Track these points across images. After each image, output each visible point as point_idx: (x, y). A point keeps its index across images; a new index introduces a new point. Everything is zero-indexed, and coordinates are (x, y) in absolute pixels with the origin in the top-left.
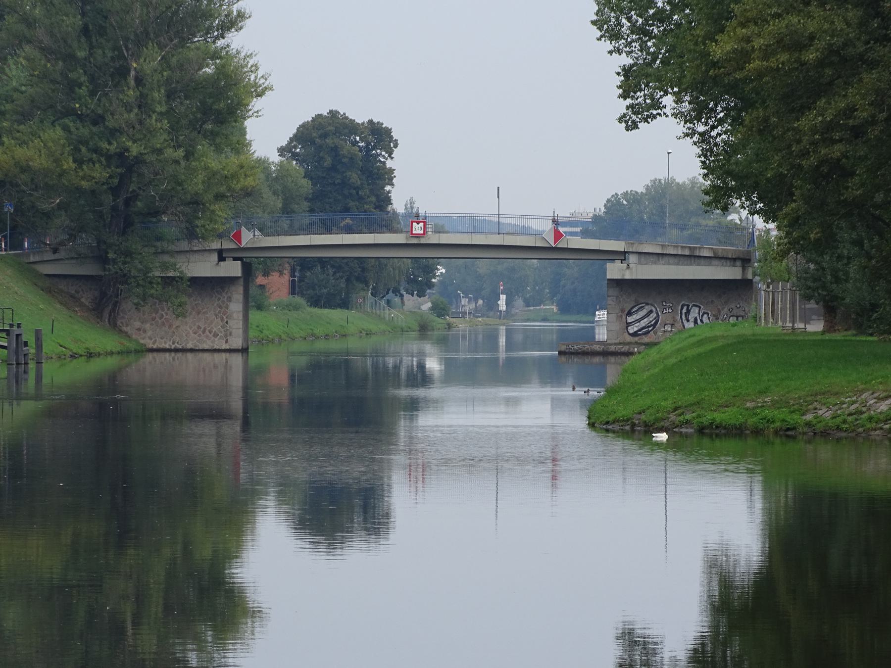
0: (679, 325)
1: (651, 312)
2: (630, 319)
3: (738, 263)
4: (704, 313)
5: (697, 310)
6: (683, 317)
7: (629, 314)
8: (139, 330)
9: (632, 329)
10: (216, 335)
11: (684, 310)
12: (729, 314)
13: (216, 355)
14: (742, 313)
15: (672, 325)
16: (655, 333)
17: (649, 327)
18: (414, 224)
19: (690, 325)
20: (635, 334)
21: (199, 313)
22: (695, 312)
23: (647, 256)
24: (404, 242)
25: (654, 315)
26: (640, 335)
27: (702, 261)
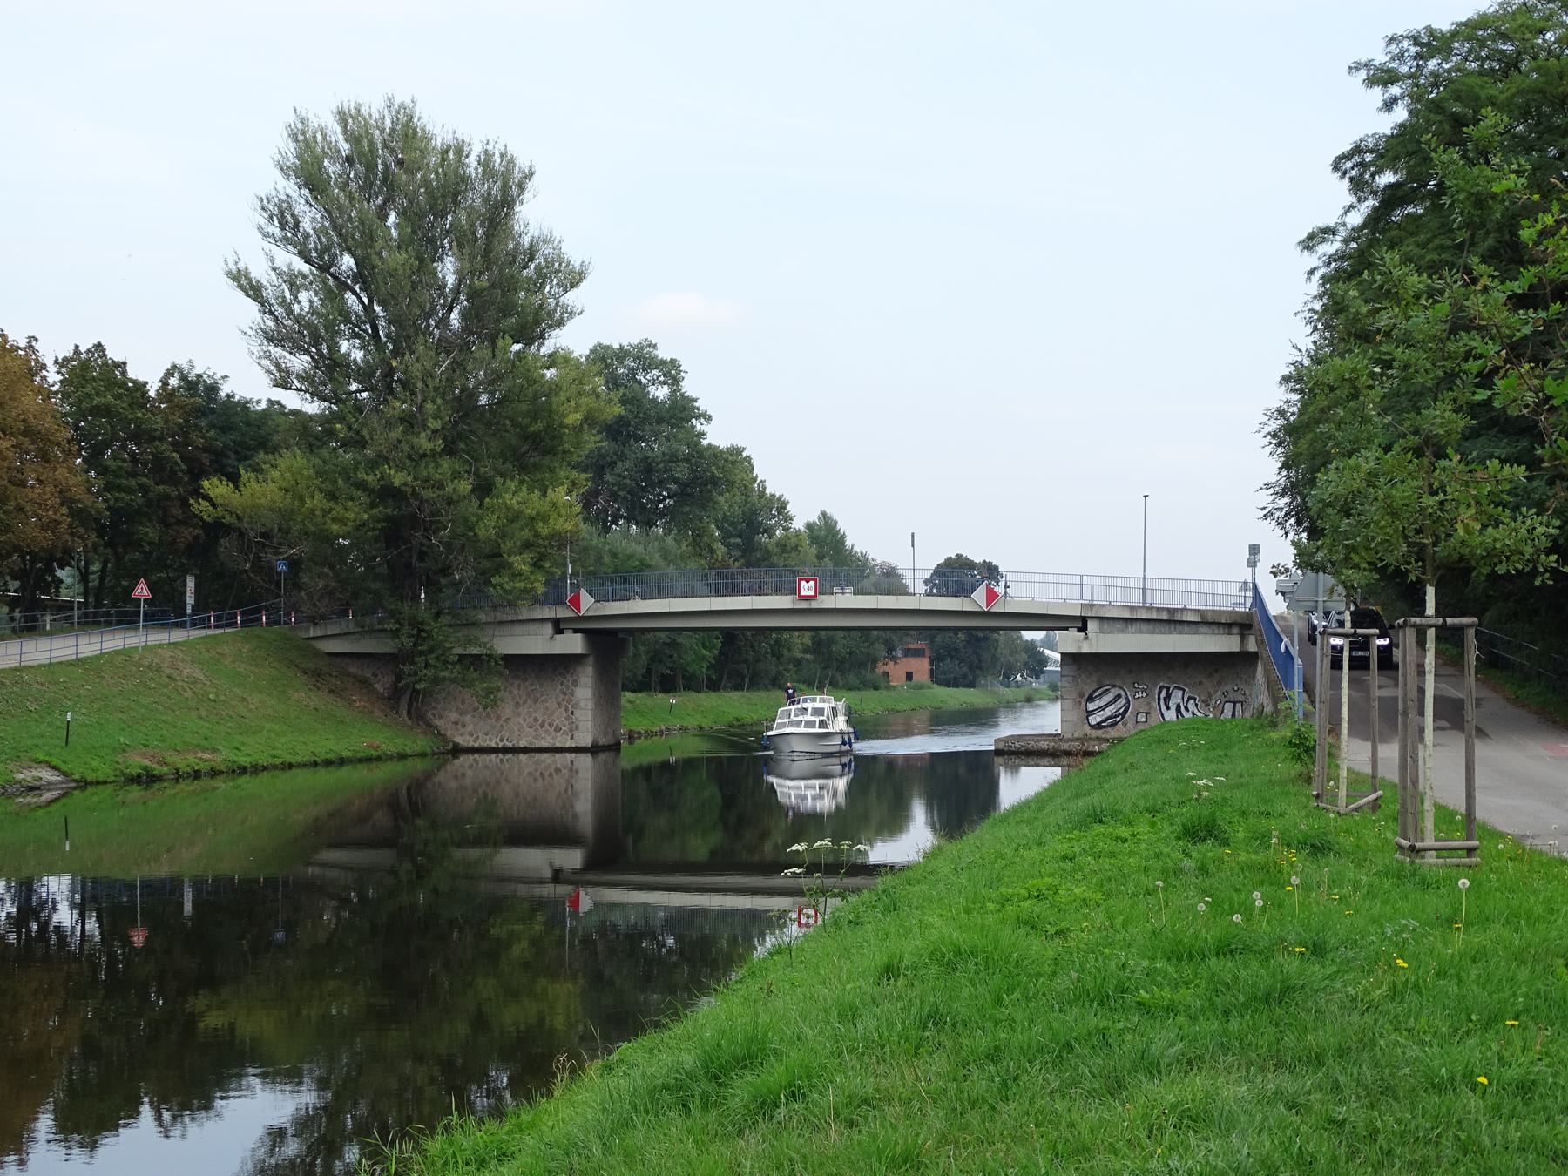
0: (1155, 715)
1: (1119, 696)
2: (1091, 707)
3: (1235, 630)
5: (1180, 693)
7: (1091, 699)
8: (456, 723)
9: (1094, 720)
10: (558, 729)
13: (558, 756)
16: (1125, 725)
18: (803, 583)
19: (1171, 715)
20: (1099, 726)
22: (1177, 697)
25: (1122, 701)
27: (1186, 628)
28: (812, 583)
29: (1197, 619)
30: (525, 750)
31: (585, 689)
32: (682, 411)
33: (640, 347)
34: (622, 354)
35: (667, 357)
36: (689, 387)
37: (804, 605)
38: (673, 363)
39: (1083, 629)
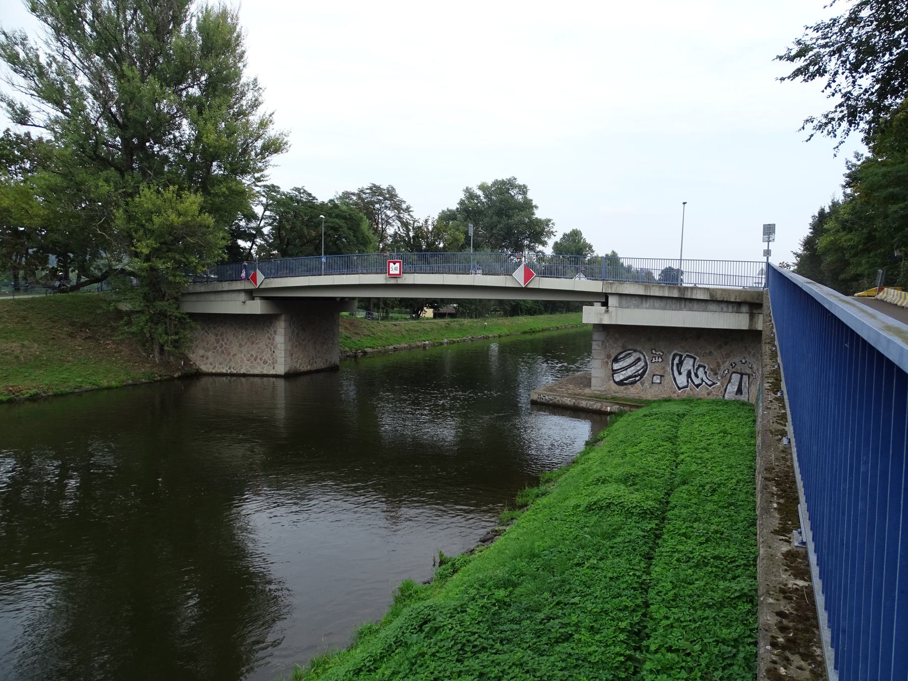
0: (668, 378)
1: (639, 360)
2: (616, 366)
3: (745, 309)
4: (700, 366)
5: (691, 361)
6: (675, 368)
7: (616, 360)
8: (203, 357)
9: (619, 377)
10: (265, 362)
11: (676, 361)
12: (731, 370)
13: (265, 379)
14: (749, 371)
15: (661, 376)
16: (642, 384)
17: (636, 376)
18: (391, 264)
19: (682, 380)
20: (620, 383)
21: (253, 343)
22: (688, 364)
23: (629, 299)
24: (383, 282)
25: (642, 364)
26: (626, 384)
27: (696, 306)
28: (398, 264)
29: (707, 297)
30: (244, 375)
31: (280, 335)
32: (528, 206)
33: (509, 180)
34: (503, 183)
35: (521, 183)
36: (530, 196)
37: (393, 282)
38: (525, 187)
39: (605, 304)
